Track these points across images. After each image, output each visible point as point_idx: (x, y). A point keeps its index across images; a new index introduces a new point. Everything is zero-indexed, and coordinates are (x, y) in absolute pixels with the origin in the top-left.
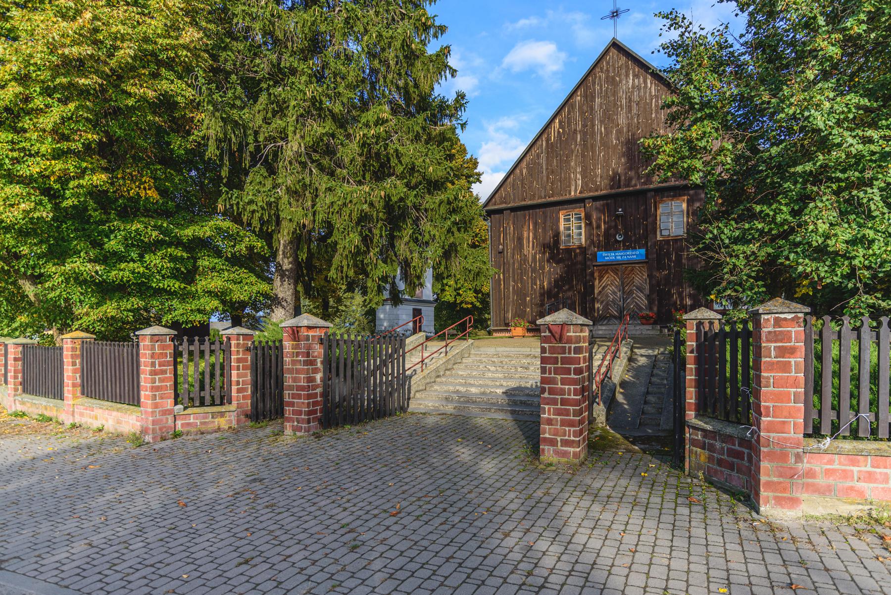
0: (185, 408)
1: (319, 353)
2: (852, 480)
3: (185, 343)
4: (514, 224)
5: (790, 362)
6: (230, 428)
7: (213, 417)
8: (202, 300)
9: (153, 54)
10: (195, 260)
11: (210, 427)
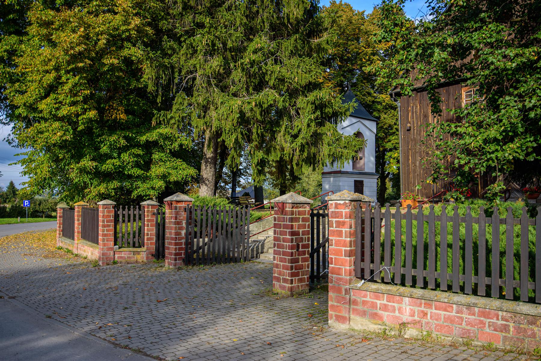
0: (120, 248)
1: (184, 217)
2: (376, 309)
3: (121, 210)
4: (420, 103)
5: (342, 231)
6: (143, 261)
7: (134, 254)
8: (154, 181)
9: (119, 35)
10: (151, 154)
11: (132, 260)
